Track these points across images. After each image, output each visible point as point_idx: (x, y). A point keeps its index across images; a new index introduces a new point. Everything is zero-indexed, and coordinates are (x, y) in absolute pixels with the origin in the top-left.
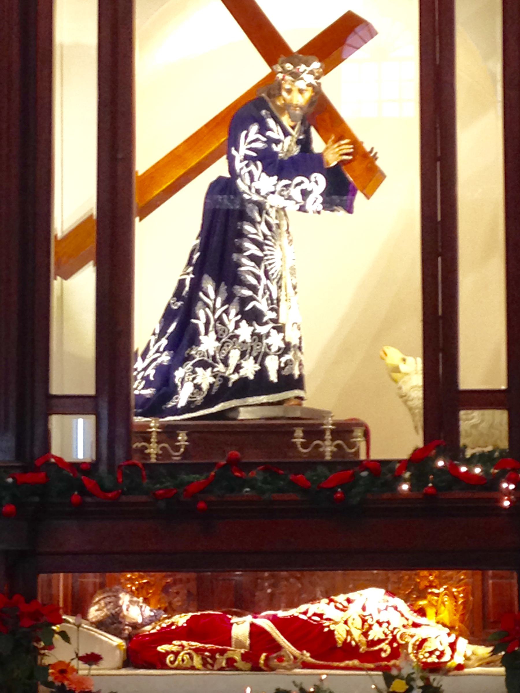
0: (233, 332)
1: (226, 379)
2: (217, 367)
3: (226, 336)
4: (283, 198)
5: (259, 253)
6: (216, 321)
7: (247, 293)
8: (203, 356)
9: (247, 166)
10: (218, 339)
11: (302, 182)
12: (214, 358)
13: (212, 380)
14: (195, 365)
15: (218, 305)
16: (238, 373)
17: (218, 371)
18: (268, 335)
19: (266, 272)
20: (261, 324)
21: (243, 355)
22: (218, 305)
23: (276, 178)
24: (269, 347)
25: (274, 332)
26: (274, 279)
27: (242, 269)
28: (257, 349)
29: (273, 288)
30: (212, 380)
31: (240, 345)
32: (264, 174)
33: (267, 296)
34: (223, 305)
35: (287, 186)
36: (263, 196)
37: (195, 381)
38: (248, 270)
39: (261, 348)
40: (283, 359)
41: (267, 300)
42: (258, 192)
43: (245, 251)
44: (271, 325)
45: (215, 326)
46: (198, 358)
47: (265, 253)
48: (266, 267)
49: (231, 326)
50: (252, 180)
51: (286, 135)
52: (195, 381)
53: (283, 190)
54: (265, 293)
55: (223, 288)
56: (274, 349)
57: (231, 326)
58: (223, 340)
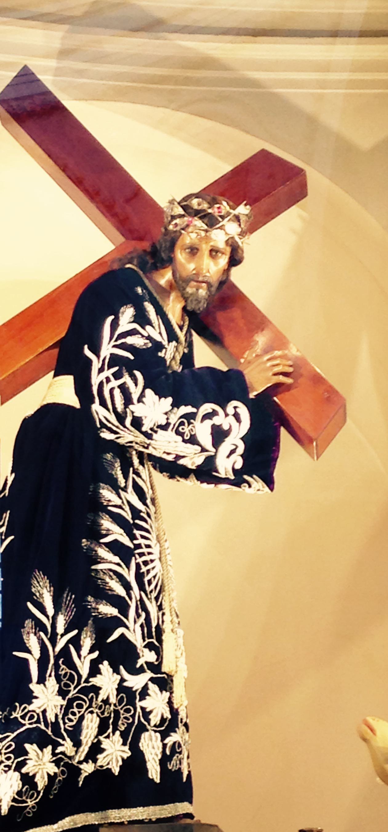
0: (87, 681)
1: (74, 771)
2: (63, 745)
3: (75, 688)
4: (180, 438)
5: (125, 540)
6: (57, 658)
7: (112, 611)
8: (38, 721)
9: (117, 376)
10: (62, 693)
11: (214, 413)
12: (55, 726)
13: (53, 769)
14: (20, 741)
15: (60, 629)
16: (95, 761)
17: (63, 753)
18: (144, 693)
19: (139, 577)
20: (136, 671)
21: (102, 728)
22: (60, 629)
23: (170, 400)
24: (146, 714)
25: (153, 688)
26: (151, 592)
27: (100, 567)
28: (126, 718)
29: (152, 607)
30: (53, 769)
31: (100, 708)
32: (149, 392)
33: (142, 620)
34: (67, 631)
35: (190, 417)
36: (146, 434)
37: (24, 770)
38: (110, 570)
39: (133, 716)
40: (169, 741)
41: (142, 626)
42: (137, 423)
43: (106, 535)
44: (149, 674)
45: (57, 666)
46: (27, 725)
47: (136, 542)
48: (138, 566)
49: (84, 669)
50: (128, 401)
51: (114, 374)
52: (24, 770)
53: (182, 424)
54: (138, 615)
55: (68, 598)
56: (155, 719)
57: (84, 669)
58: (70, 695)
